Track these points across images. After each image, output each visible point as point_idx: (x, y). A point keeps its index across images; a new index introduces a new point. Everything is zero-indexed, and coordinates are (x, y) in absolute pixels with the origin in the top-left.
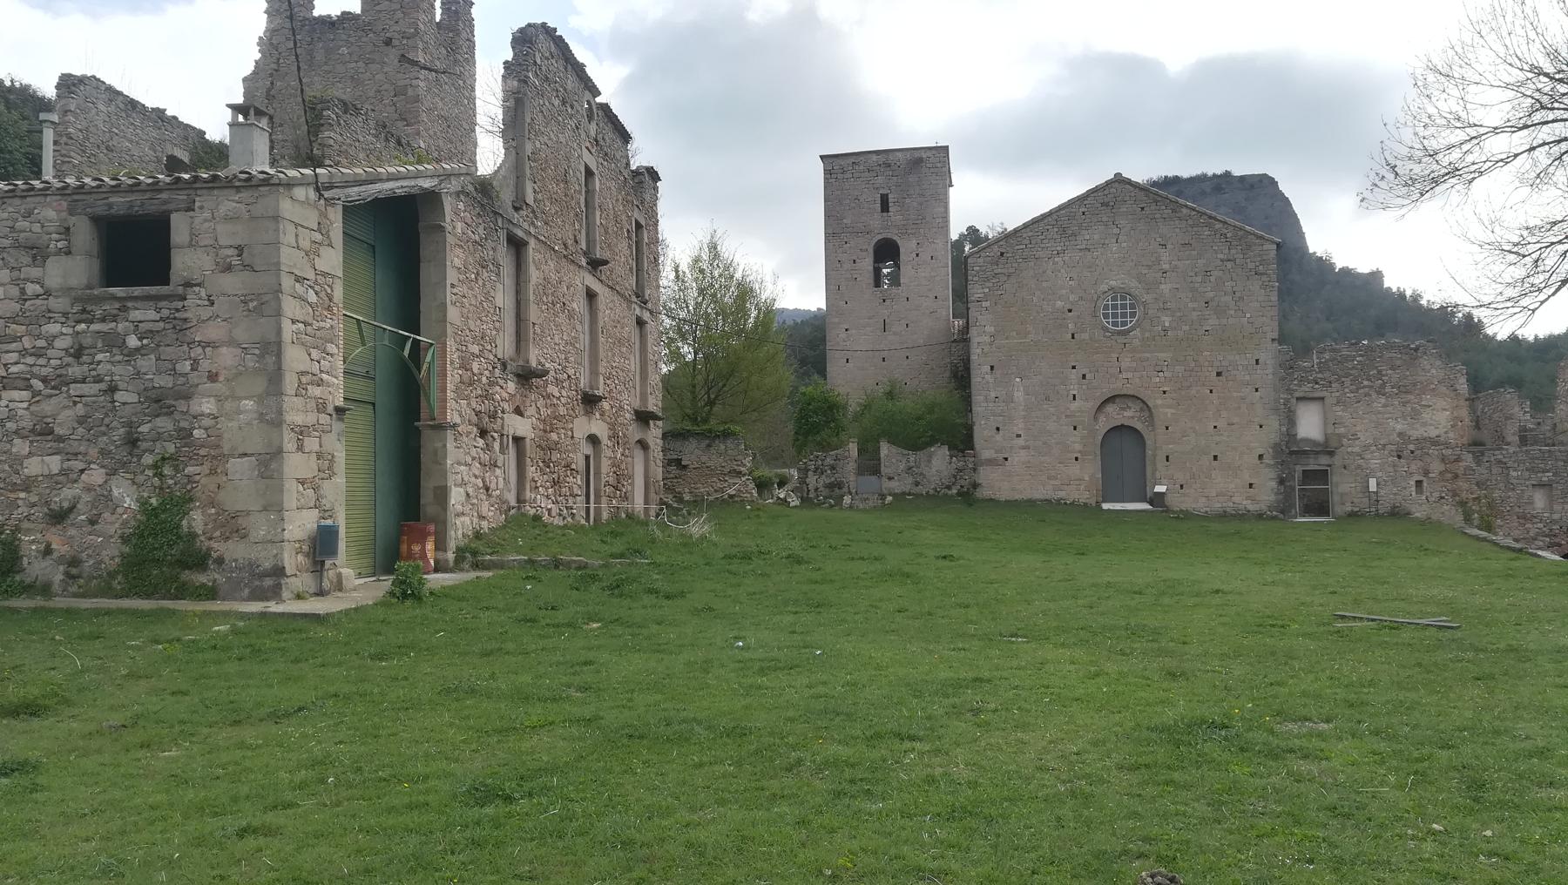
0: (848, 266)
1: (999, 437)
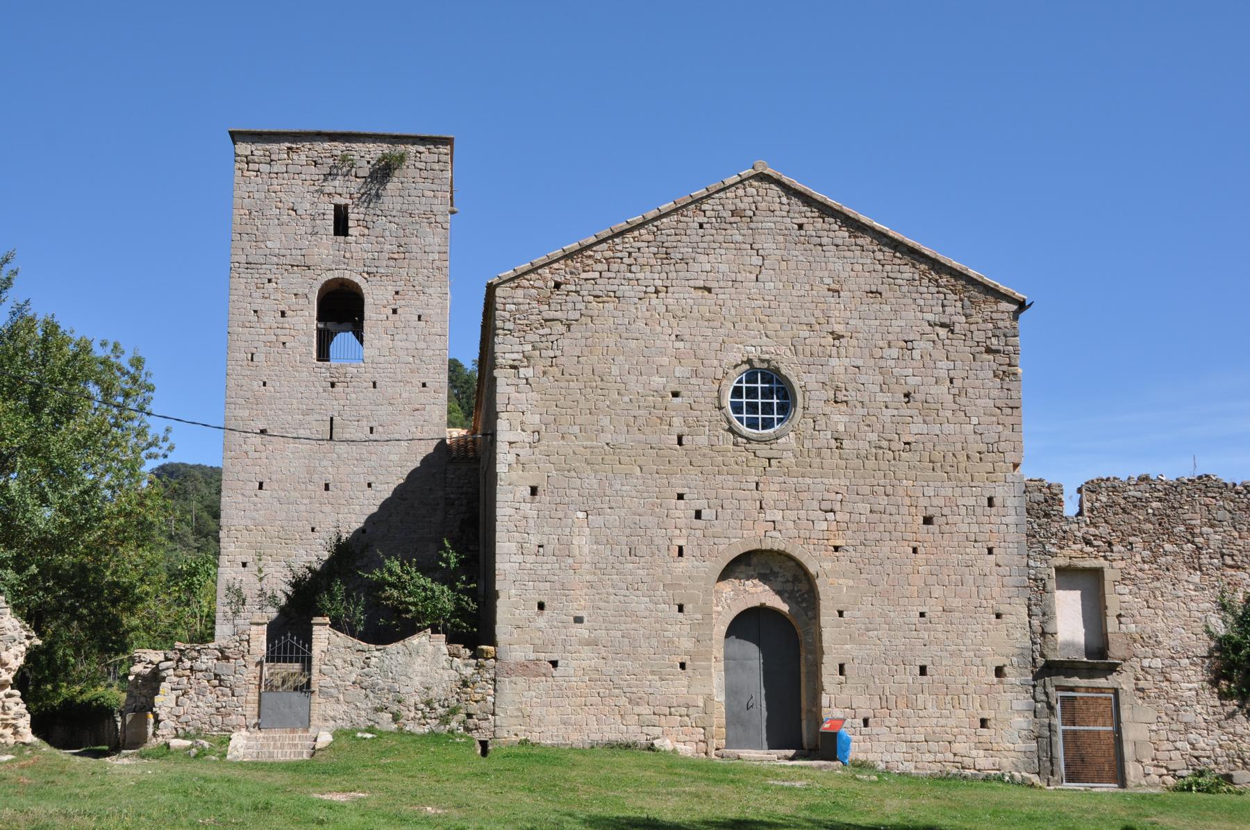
1: (542, 621)
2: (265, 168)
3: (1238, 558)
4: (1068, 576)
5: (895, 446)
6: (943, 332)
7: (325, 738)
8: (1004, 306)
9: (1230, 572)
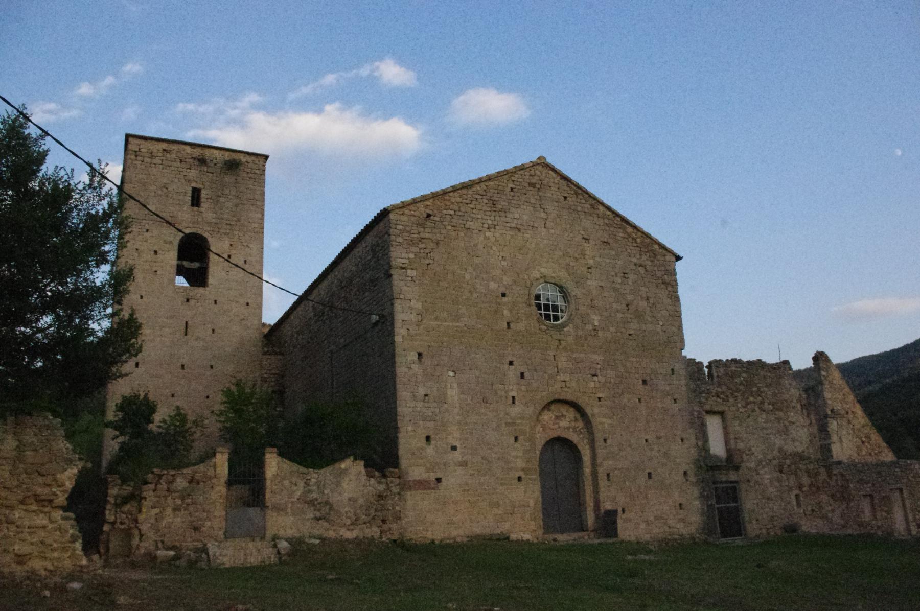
0: (150, 256)
1: (430, 450)
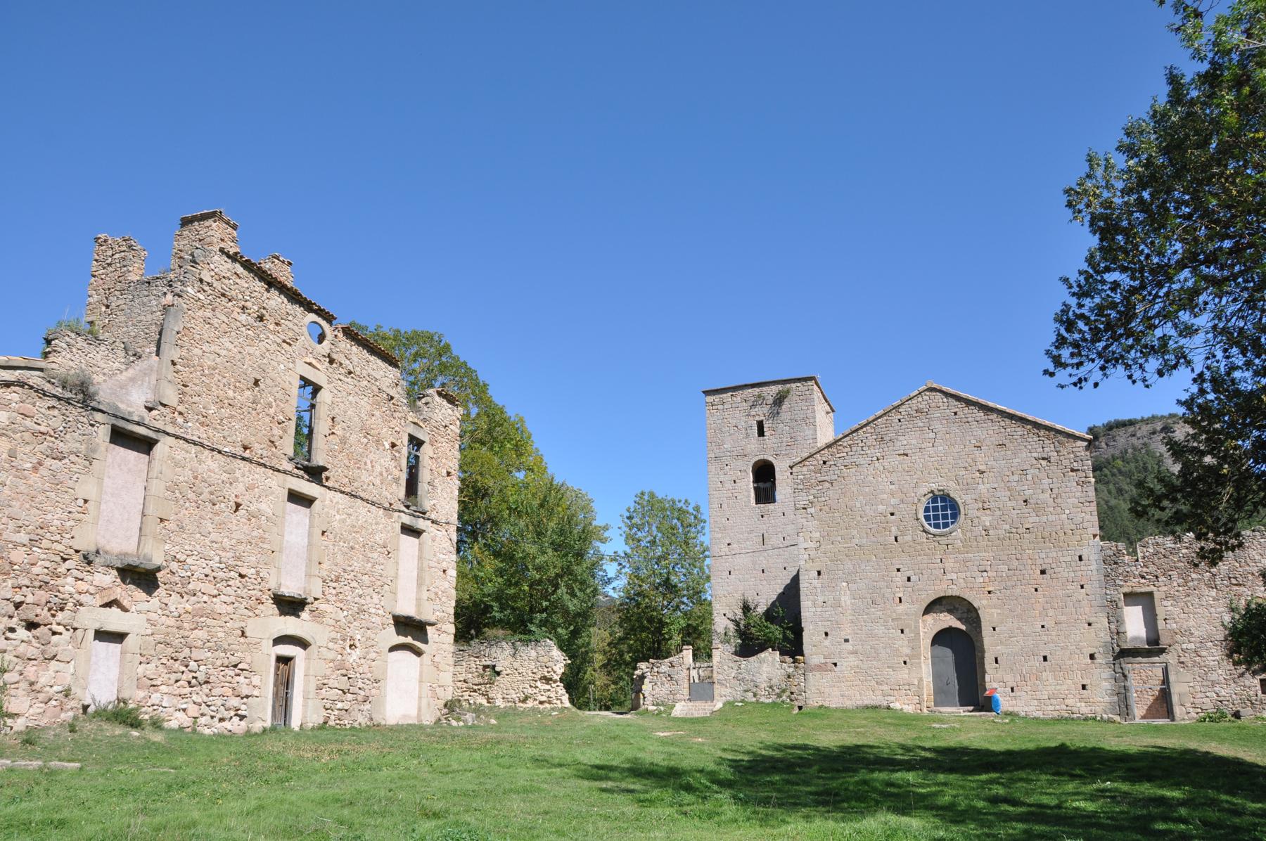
1: (827, 642)
2: (720, 407)
3: (1240, 579)
4: (1131, 598)
5: (1020, 531)
6: (1044, 463)
7: (719, 705)
8: (1080, 443)
9: (1235, 588)
